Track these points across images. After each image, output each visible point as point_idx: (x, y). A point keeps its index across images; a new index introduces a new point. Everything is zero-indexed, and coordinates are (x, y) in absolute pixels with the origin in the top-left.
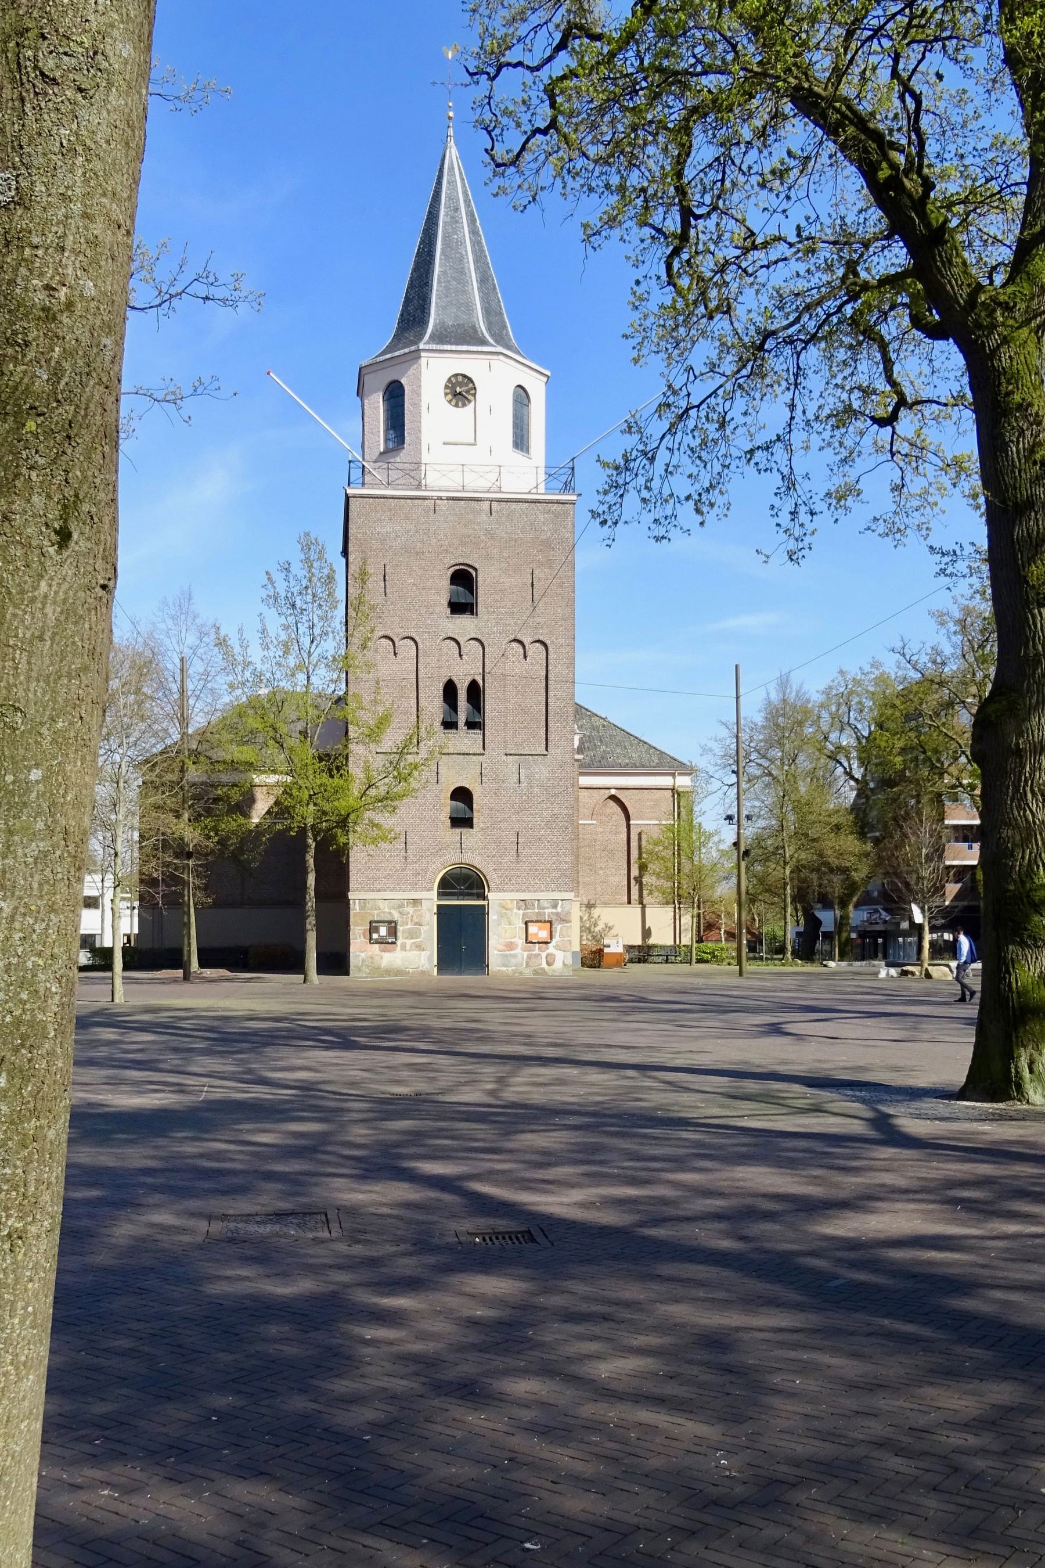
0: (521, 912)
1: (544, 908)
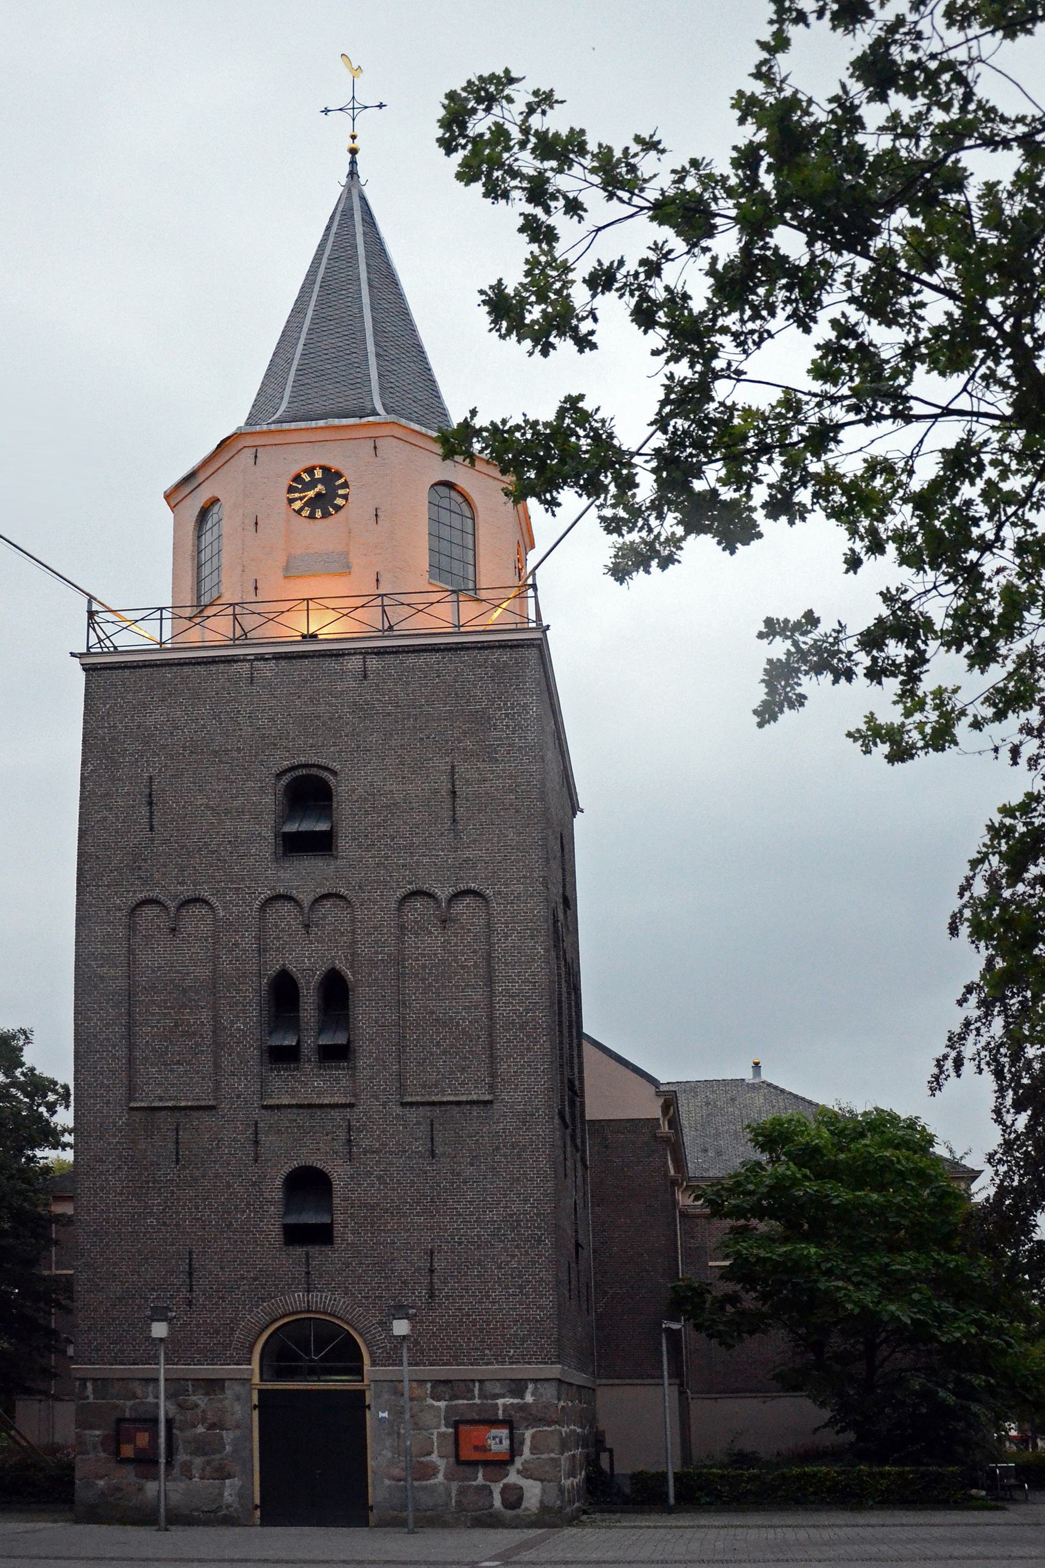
0: (442, 1404)
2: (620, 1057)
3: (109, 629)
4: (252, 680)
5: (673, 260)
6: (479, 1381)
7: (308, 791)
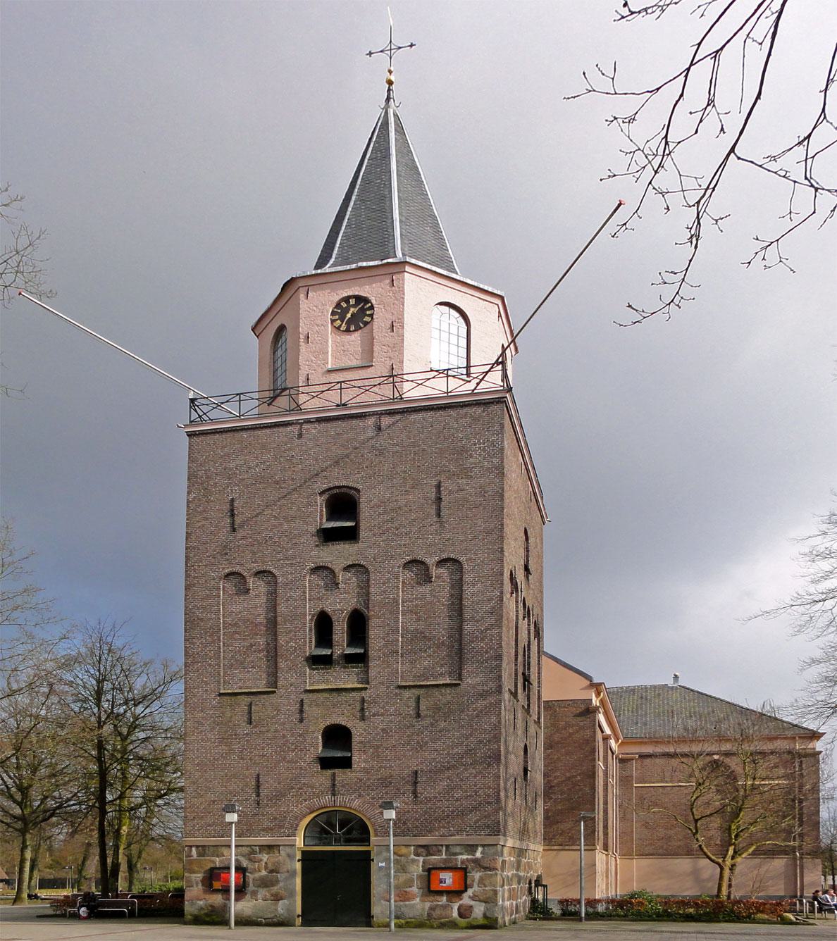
0: (421, 859)
1: (456, 854)
2: (567, 664)
3: (205, 409)
4: (300, 436)
5: (662, 139)
6: (446, 845)
7: (343, 504)
